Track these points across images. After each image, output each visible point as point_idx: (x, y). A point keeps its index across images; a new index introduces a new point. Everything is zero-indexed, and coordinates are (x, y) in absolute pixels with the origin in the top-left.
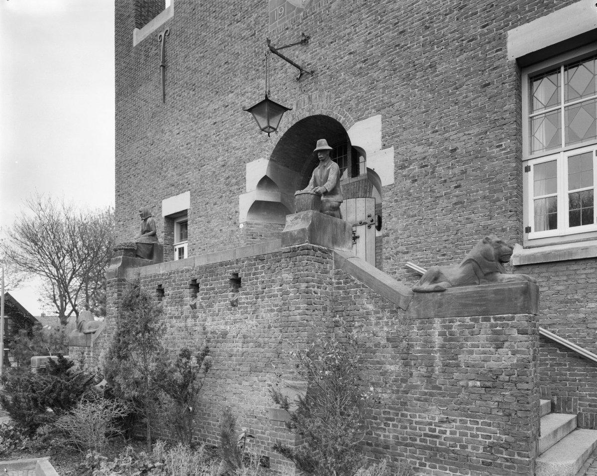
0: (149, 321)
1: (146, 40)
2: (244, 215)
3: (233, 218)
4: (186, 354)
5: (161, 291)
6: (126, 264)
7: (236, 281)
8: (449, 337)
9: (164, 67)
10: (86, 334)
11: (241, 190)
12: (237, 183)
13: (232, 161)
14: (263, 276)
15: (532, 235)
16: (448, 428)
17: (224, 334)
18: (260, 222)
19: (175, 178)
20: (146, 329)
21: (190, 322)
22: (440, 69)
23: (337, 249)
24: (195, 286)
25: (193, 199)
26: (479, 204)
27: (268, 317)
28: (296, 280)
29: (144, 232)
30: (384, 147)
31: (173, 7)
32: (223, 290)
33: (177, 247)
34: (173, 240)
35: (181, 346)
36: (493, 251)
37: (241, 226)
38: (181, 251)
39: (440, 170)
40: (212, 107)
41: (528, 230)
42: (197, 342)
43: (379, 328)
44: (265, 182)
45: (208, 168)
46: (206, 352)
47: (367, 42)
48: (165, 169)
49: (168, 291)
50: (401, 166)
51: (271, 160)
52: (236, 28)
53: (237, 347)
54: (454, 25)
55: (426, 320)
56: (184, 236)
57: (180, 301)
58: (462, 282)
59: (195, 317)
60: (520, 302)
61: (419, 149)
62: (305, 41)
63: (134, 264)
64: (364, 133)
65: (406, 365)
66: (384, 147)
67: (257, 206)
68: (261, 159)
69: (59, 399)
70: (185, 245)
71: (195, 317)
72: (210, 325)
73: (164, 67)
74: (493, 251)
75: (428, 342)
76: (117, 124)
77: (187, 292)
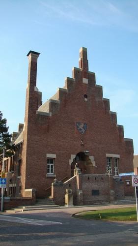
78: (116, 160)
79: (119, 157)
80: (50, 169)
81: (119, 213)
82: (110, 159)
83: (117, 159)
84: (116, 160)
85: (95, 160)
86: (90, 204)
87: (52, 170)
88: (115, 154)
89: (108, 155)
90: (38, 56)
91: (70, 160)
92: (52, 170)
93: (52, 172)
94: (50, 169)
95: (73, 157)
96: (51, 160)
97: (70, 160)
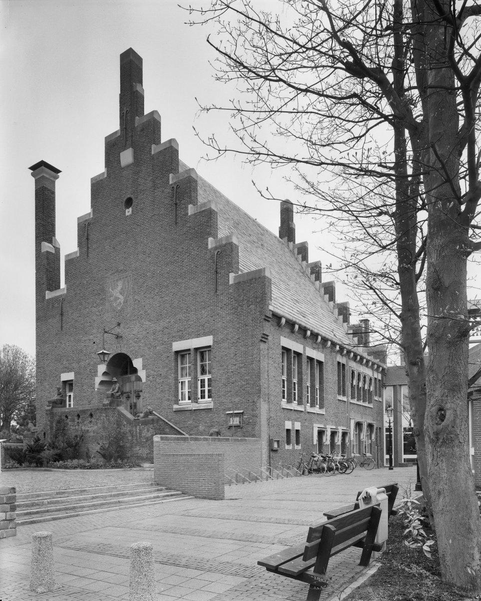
0: (65, 427)
1: (52, 298)
2: (97, 386)
3: (92, 386)
4: (76, 436)
5: (67, 417)
6: (53, 407)
7: (91, 415)
8: (140, 430)
9: (62, 315)
10: (32, 432)
11: (96, 375)
12: (94, 372)
13: (92, 363)
14: (99, 414)
15: (181, 402)
16: (140, 451)
17: (88, 431)
18: (103, 388)
19: (67, 365)
20: (64, 430)
21: (77, 427)
22: (158, 348)
23: (118, 408)
24: (79, 416)
25: (75, 376)
26: (167, 392)
27: (99, 425)
28: (106, 416)
29: (58, 395)
30: (143, 369)
31: (66, 289)
32: (88, 417)
33: (68, 395)
34: (66, 391)
35: (74, 435)
36: (148, 411)
37: (96, 390)
38: (70, 396)
39: (158, 380)
40: (84, 339)
41: (199, 399)
42: (79, 433)
43: (126, 429)
44: (105, 374)
45: (82, 363)
46: (82, 436)
47: (138, 332)
48: (62, 360)
49: (69, 417)
50: (148, 377)
51: (107, 365)
52: (94, 309)
53: (92, 434)
54: (161, 336)
55: (136, 426)
56: (71, 390)
57: (73, 421)
58: (143, 418)
59: (78, 426)
60: (151, 422)
61: (152, 372)
62: (119, 324)
63: (55, 407)
64: (137, 363)
65: (132, 437)
66: (143, 369)
67: (102, 383)
68: (104, 365)
69: (457, 201)
70: (72, 394)
71: (78, 426)
72: (83, 428)
73: (62, 315)
74: (148, 411)
75: (136, 432)
76: (37, 333)
77: (76, 418)
78: (202, 354)
79: (211, 343)
80: (206, 388)
81: (36, 250)
82: (181, 354)
83: (201, 352)
84: (202, 354)
85: (144, 367)
86: (134, 156)
87: (203, 386)
88: (198, 336)
89: (178, 346)
90: (57, 177)
91: (96, 378)
92: (203, 386)
93: (203, 381)
94: (206, 388)
95: (102, 368)
96: (69, 384)
97: (96, 378)
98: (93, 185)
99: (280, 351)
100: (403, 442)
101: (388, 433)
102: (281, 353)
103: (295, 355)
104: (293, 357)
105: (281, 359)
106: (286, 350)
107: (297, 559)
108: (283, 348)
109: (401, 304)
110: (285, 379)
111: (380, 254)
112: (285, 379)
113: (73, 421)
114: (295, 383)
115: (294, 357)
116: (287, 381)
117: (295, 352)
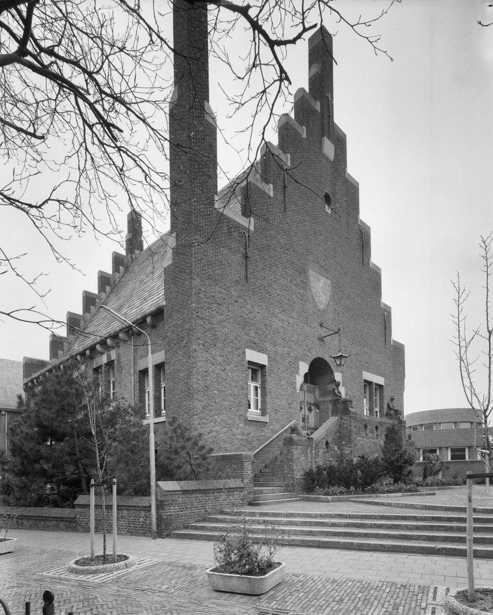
24: (377, 428)
98: (403, 345)
99: (363, 384)
100: (258, 511)
101: (487, 480)
102: (363, 386)
103: (366, 384)
104: (374, 389)
105: (363, 391)
106: (368, 383)
107: (376, 555)
108: (365, 381)
109: (29, 41)
110: (259, 386)
111: (233, 105)
112: (259, 386)
113: (372, 432)
114: (377, 412)
115: (376, 388)
116: (380, 411)
117: (376, 384)
